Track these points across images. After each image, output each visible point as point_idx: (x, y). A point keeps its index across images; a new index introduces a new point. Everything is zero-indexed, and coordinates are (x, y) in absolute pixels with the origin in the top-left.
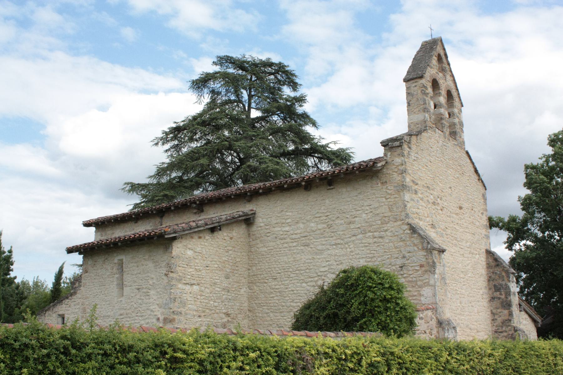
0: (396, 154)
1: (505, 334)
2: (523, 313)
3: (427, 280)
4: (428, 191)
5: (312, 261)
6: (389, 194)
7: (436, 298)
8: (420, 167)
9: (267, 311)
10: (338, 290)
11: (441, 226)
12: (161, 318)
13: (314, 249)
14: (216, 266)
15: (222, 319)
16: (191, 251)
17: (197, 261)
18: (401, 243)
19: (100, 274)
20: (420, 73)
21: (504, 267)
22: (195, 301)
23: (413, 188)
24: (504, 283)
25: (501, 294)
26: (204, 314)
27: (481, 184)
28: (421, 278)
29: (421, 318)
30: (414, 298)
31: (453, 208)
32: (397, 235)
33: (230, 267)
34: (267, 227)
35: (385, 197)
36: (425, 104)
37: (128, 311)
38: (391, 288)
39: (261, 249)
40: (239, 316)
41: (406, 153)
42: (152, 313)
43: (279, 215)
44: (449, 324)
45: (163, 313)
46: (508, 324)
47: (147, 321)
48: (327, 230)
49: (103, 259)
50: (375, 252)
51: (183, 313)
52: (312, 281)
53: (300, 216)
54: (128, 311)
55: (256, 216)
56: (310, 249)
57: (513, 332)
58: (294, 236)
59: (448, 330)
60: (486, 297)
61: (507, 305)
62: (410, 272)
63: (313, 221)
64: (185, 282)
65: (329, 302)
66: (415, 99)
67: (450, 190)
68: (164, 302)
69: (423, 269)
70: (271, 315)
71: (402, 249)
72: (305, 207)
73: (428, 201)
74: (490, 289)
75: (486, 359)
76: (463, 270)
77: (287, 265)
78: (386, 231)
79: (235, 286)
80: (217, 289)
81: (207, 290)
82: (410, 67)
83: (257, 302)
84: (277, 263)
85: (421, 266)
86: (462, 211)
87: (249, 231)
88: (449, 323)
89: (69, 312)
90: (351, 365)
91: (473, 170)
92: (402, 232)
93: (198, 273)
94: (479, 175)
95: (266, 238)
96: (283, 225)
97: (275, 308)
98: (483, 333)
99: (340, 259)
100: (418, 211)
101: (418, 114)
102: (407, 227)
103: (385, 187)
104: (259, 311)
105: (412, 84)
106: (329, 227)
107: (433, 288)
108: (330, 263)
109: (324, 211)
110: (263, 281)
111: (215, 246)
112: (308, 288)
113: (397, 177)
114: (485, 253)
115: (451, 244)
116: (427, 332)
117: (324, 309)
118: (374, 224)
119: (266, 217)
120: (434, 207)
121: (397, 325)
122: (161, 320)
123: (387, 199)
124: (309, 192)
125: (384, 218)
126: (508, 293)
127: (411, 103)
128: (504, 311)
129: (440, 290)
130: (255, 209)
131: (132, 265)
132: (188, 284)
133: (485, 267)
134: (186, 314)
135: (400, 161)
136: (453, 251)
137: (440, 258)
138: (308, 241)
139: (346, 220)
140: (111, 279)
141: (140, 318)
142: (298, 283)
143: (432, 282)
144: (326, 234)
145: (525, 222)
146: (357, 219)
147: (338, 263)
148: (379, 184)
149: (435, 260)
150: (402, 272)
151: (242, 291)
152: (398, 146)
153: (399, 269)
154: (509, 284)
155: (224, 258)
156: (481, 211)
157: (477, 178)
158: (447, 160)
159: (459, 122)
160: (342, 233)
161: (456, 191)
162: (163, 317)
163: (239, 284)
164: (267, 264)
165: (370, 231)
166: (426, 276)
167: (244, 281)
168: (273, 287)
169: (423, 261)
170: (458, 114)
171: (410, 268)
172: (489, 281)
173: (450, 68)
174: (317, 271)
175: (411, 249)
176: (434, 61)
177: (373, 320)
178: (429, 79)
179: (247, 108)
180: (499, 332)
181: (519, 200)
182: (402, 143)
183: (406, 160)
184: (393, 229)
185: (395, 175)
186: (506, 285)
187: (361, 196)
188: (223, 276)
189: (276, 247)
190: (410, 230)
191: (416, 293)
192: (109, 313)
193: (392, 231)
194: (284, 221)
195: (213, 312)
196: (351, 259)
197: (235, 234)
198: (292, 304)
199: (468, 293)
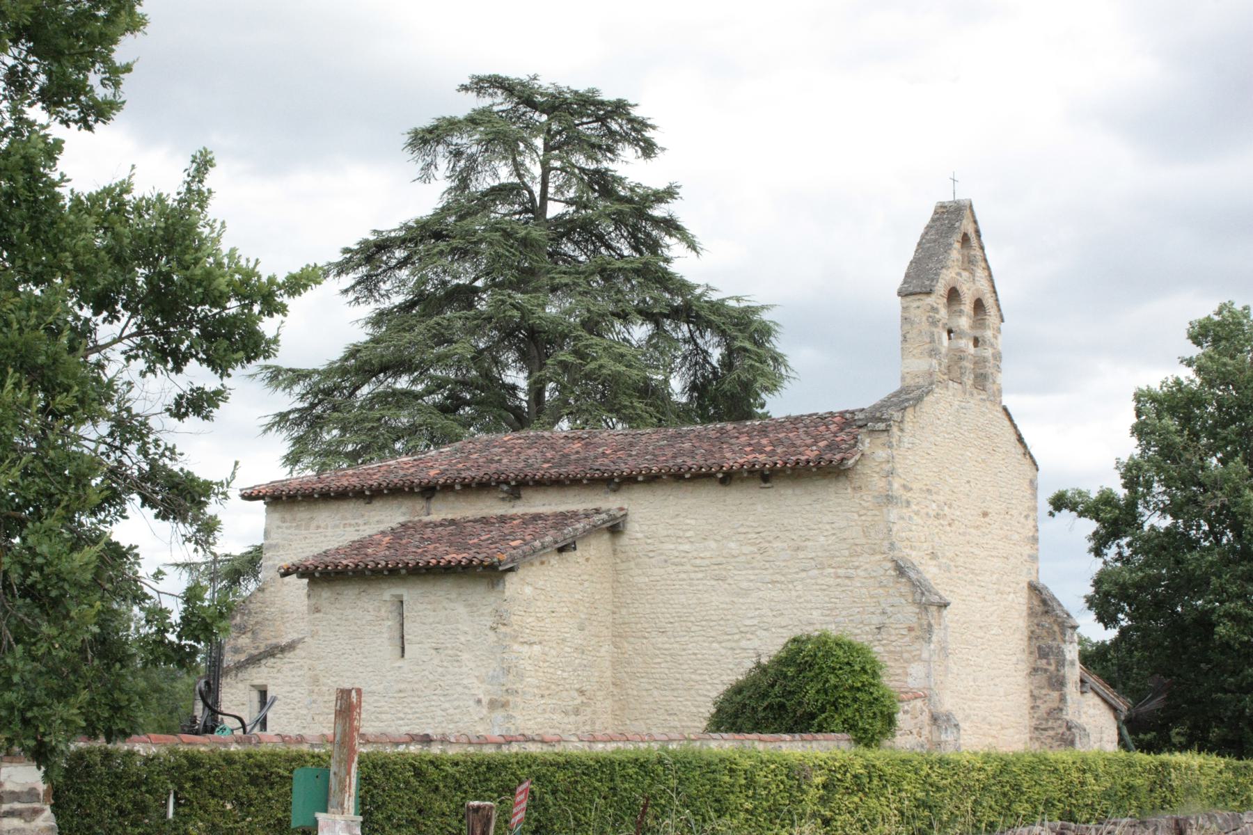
0: (879, 442)
1: (1051, 733)
2: (1090, 695)
3: (918, 652)
4: (929, 497)
5: (730, 606)
6: (864, 508)
7: (930, 681)
8: (917, 458)
9: (648, 687)
10: (784, 669)
11: (948, 554)
12: (485, 700)
13: (734, 586)
14: (566, 610)
15: (574, 699)
16: (530, 588)
17: (539, 603)
18: (881, 591)
19: (351, 617)
20: (927, 283)
21: (1057, 616)
22: (537, 671)
23: (904, 498)
24: (1054, 644)
25: (1049, 664)
26: (548, 692)
27: (1029, 461)
28: (908, 648)
29: (906, 712)
30: (897, 678)
31: (970, 518)
32: (875, 577)
33: (585, 611)
34: (649, 541)
35: (857, 512)
36: (932, 341)
37: (417, 686)
38: (864, 670)
39: (637, 579)
40: (599, 693)
41: (894, 441)
42: (467, 691)
43: (671, 522)
44: (949, 720)
45: (487, 692)
46: (1056, 716)
47: (456, 703)
48: (759, 557)
49: (357, 591)
50: (837, 601)
51: (520, 691)
52: (729, 640)
53: (710, 527)
54: (417, 686)
55: (629, 519)
56: (727, 586)
57: (1064, 729)
58: (698, 562)
59: (946, 729)
60: (1024, 668)
61: (1058, 683)
62: (893, 638)
63: (734, 538)
64: (522, 640)
65: (772, 686)
66: (915, 331)
67: (967, 485)
68: (490, 674)
69: (913, 634)
70: (656, 693)
71: (882, 600)
72: (720, 513)
73: (927, 514)
74: (1031, 653)
75: (974, 774)
76: (982, 624)
77: (685, 611)
78: (857, 568)
79: (592, 643)
80: (567, 649)
81: (552, 651)
82: (911, 263)
83: (628, 670)
84: (669, 606)
85: (911, 629)
86: (987, 519)
87: (613, 544)
88: (948, 718)
89: (279, 681)
90: (839, 776)
91: (1014, 438)
92: (882, 572)
93: (540, 624)
94: (1025, 446)
95: (647, 560)
96: (679, 540)
97: (662, 682)
98: (1012, 730)
99: (778, 607)
100: (911, 534)
101: (919, 358)
102: (890, 565)
103: (859, 495)
104: (633, 686)
105: (913, 302)
106: (763, 551)
107: (926, 664)
108: (763, 612)
109: (753, 524)
110: (640, 634)
111: (564, 575)
112: (723, 651)
113: (878, 483)
114: (1026, 590)
115: (963, 582)
116: (914, 731)
117: (765, 695)
118: (838, 554)
119: (648, 523)
120: (936, 523)
121: (869, 724)
122: (484, 703)
123: (860, 516)
124: (727, 489)
125: (855, 547)
126: (1061, 663)
127: (908, 336)
128: (1052, 693)
129: (937, 667)
130: (626, 506)
131: (421, 607)
132: (525, 643)
133: (1025, 614)
134: (524, 693)
135: (884, 455)
136: (966, 593)
137: (940, 617)
138: (724, 573)
139: (791, 543)
140: (376, 628)
141: (442, 699)
142: (704, 641)
143: (925, 655)
144: (755, 564)
145: (1131, 504)
146: (809, 544)
147: (775, 613)
148: (849, 490)
149: (932, 622)
150: (879, 637)
151: (603, 650)
152: (883, 431)
153: (876, 631)
154: (1063, 646)
155: (576, 596)
156: (1025, 513)
157: (1022, 451)
158: (966, 433)
159: (993, 354)
160: (784, 564)
161: (979, 486)
162: (489, 698)
163: (597, 639)
164: (648, 606)
165: (830, 566)
166: (917, 646)
167: (605, 632)
168: (660, 645)
169: (914, 621)
170: (993, 340)
171: (893, 632)
172: (1030, 638)
173: (984, 254)
174: (739, 624)
175: (896, 600)
176: (955, 253)
177: (836, 716)
178: (942, 292)
179: (538, 200)
180: (1042, 729)
181: (1117, 468)
182: (890, 425)
183: (895, 453)
184: (867, 566)
185: (876, 477)
186: (1059, 647)
187: (818, 506)
188: (576, 626)
189: (665, 577)
190: (895, 570)
191: (899, 671)
192: (373, 688)
193: (866, 570)
194: (681, 534)
195: (561, 688)
196: (797, 609)
197: (593, 552)
198: (693, 676)
199: (988, 662)
